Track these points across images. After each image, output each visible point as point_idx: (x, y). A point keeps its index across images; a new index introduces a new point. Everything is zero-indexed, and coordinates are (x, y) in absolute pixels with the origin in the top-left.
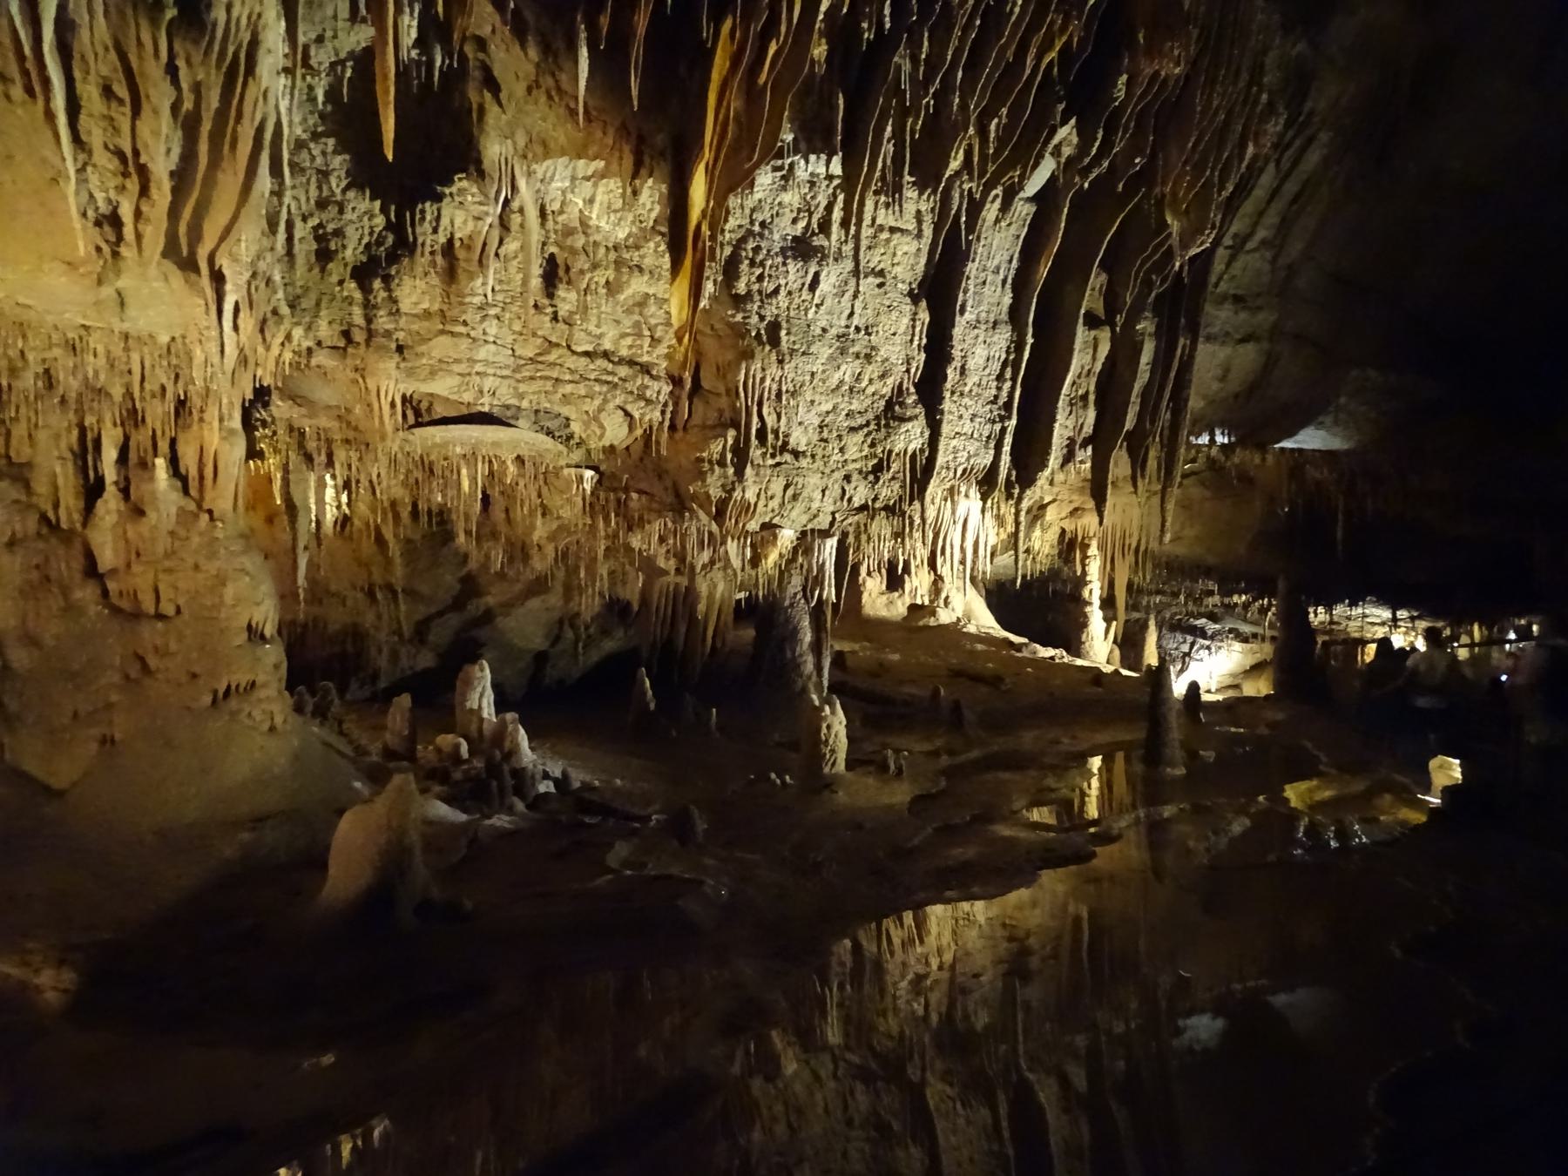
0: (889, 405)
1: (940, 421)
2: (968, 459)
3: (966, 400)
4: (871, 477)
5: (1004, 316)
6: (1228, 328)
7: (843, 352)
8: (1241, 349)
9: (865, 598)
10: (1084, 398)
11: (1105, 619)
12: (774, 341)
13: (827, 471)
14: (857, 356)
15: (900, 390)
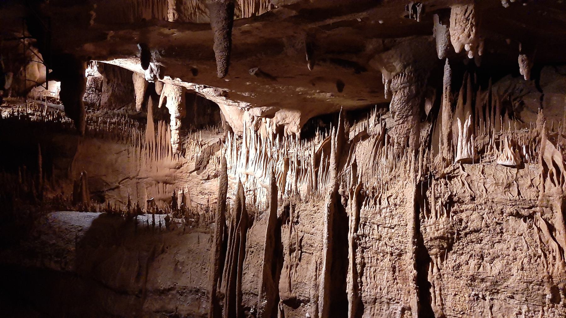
0: (450, 248)
1: (414, 237)
2: (380, 211)
3: (389, 249)
4: (455, 199)
5: (368, 307)
6: (182, 298)
7: (495, 283)
8: (169, 284)
9: (298, 122)
10: (292, 251)
11: (167, 109)
12: (554, 290)
13: (489, 203)
14: (483, 280)
15: (443, 257)
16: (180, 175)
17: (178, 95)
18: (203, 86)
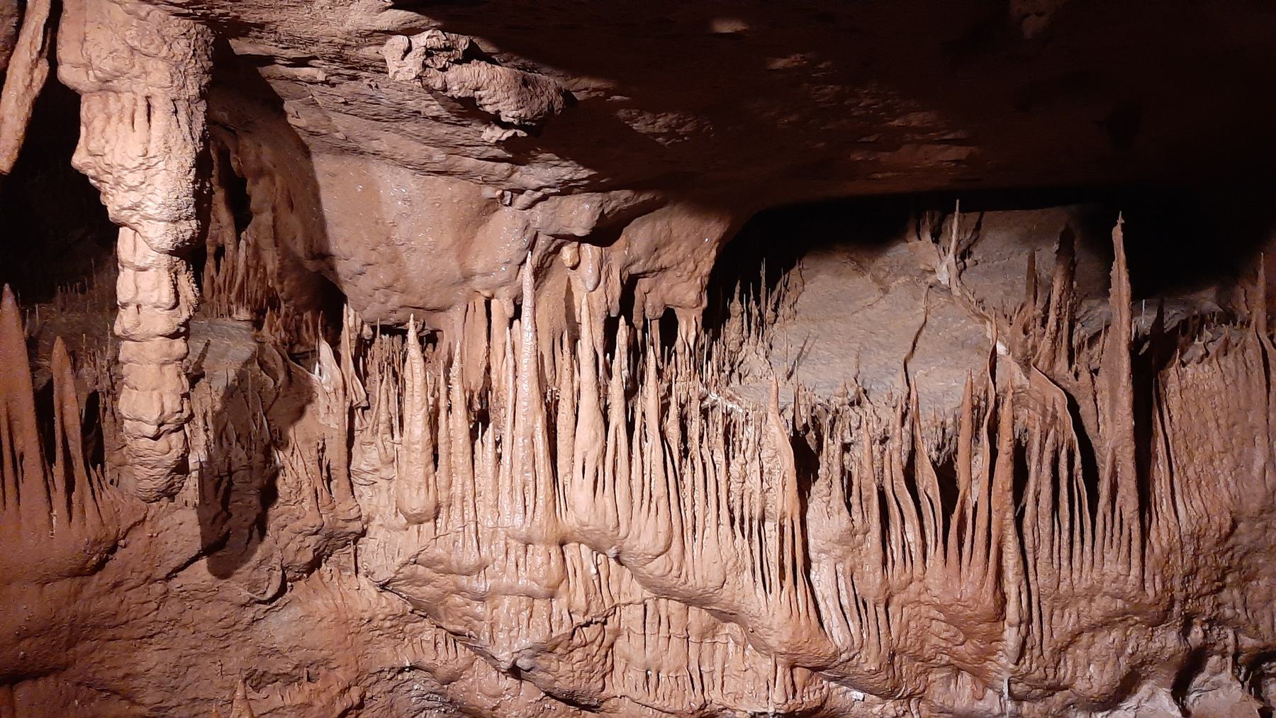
16: (110, 603)
17: (193, 91)
18: (463, 42)
